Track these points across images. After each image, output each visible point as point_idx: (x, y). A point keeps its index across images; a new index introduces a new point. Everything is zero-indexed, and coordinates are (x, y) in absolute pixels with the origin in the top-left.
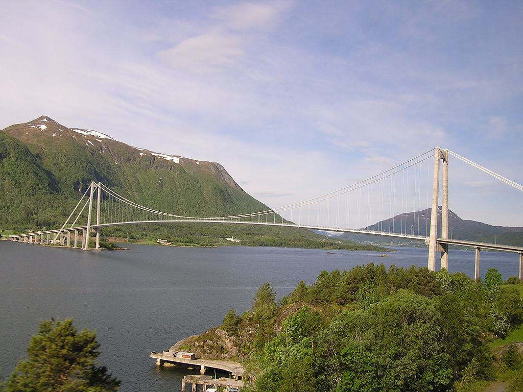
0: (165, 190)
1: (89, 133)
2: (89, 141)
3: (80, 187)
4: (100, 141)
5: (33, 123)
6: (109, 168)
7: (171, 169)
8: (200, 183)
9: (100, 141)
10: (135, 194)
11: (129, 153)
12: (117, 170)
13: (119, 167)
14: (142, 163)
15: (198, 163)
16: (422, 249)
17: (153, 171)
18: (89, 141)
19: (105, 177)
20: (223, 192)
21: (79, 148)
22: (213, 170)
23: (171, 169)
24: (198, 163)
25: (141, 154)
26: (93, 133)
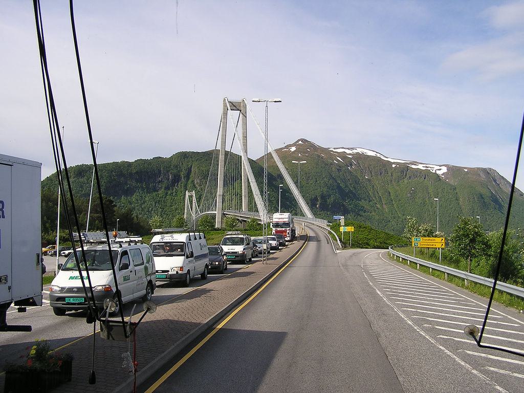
0: (417, 200)
1: (355, 151)
2: (338, 158)
3: (318, 203)
4: (350, 156)
5: (286, 147)
6: (357, 182)
7: (425, 178)
8: (457, 190)
9: (350, 156)
10: (385, 206)
11: (379, 166)
12: (366, 184)
13: (369, 180)
14: (394, 175)
15: (466, 170)
16: (437, 265)
17: (406, 181)
18: (338, 158)
19: (351, 192)
20: (483, 198)
21: (323, 165)
22: (483, 176)
23: (425, 178)
24: (466, 170)
25: (394, 166)
26: (359, 151)
